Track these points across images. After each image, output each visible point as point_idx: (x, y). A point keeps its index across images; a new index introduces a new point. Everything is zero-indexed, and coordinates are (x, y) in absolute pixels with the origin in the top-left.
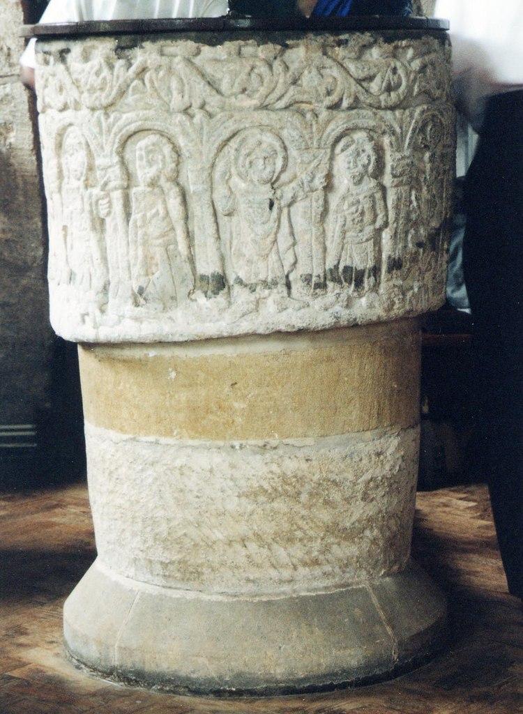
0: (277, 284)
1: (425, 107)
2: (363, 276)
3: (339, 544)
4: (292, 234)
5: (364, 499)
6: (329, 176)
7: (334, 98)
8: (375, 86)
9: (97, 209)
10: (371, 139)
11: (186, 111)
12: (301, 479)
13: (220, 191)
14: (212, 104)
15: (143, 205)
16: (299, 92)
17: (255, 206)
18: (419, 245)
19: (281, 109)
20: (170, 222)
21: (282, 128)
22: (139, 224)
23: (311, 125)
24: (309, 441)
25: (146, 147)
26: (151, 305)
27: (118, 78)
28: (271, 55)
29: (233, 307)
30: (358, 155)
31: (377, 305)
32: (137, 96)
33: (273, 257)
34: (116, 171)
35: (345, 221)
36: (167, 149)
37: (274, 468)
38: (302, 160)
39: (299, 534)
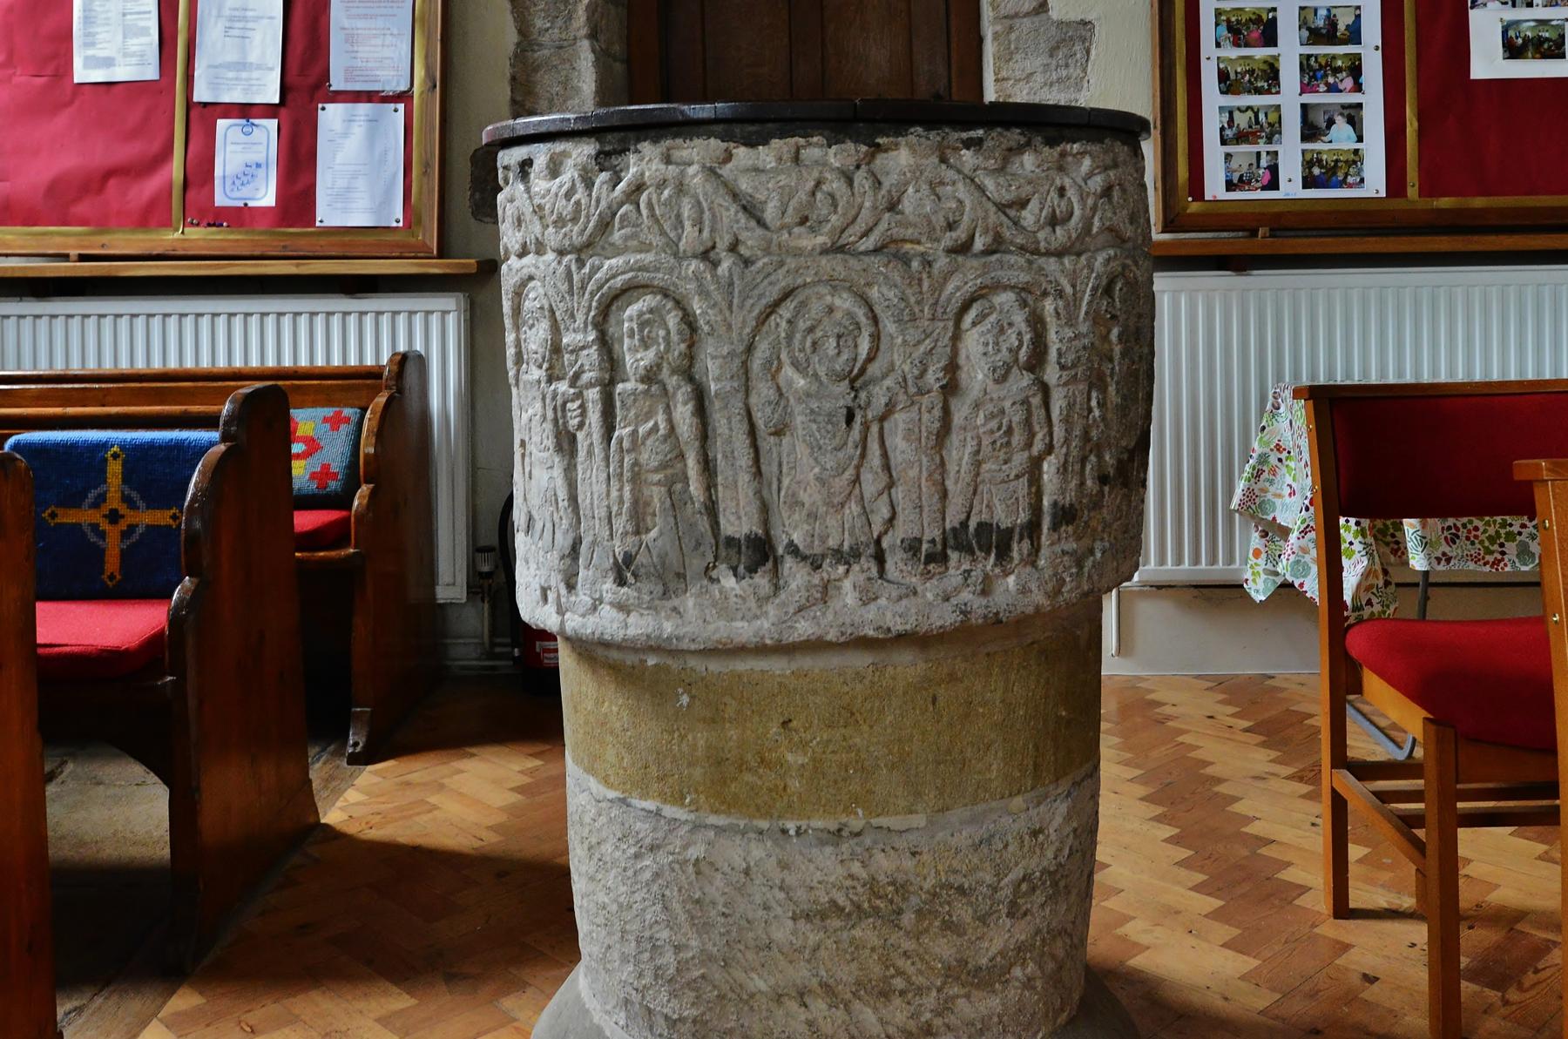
0: (859, 556)
1: (1112, 252)
2: (1011, 538)
3: (968, 996)
4: (887, 467)
5: (1010, 915)
6: (952, 367)
7: (960, 234)
8: (1028, 217)
9: (564, 417)
10: (1024, 304)
11: (707, 255)
12: (902, 888)
13: (763, 391)
14: (749, 243)
16: (899, 224)
17: (820, 419)
18: (1103, 479)
19: (866, 253)
20: (677, 444)
21: (869, 284)
22: (626, 445)
23: (920, 280)
24: (919, 820)
26: (646, 586)
27: (598, 201)
28: (850, 163)
29: (783, 596)
30: (1002, 331)
31: (1033, 586)
32: (627, 231)
33: (854, 508)
34: (591, 356)
35: (979, 444)
36: (673, 320)
37: (856, 868)
38: (905, 341)
39: (899, 983)
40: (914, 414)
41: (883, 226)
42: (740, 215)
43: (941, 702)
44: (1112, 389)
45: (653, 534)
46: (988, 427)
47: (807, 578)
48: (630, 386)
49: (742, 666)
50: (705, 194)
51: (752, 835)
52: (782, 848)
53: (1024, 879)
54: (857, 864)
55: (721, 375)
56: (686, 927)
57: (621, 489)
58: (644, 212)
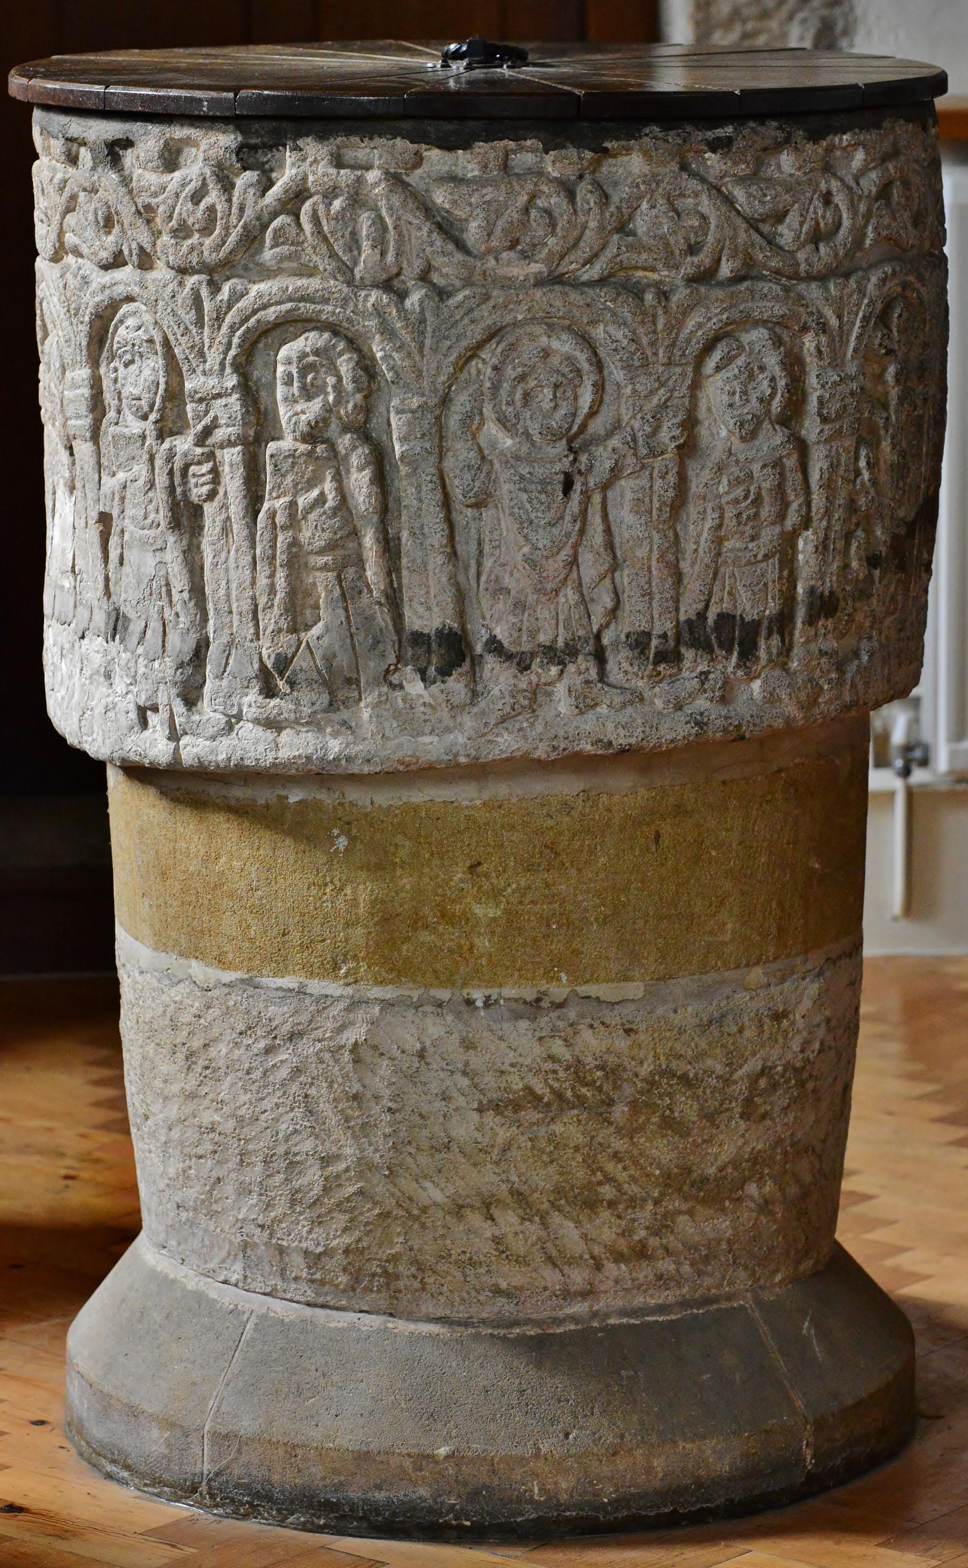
1: (888, 269)
2: (757, 634)
3: (690, 1213)
4: (610, 545)
5: (744, 1116)
6: (690, 423)
7: (704, 258)
8: (786, 233)
9: (185, 482)
10: (778, 342)
12: (613, 1073)
13: (460, 453)
15: (289, 479)
16: (630, 247)
18: (873, 561)
19: (590, 284)
21: (593, 323)
22: (280, 519)
23: (654, 316)
24: (635, 989)
27: (242, 209)
33: (569, 594)
35: (721, 517)
36: (345, 365)
37: (558, 1047)
38: (634, 391)
39: (607, 1191)
40: (644, 481)
41: (611, 251)
42: (435, 235)
43: (666, 841)
44: (886, 446)
45: (316, 630)
46: (732, 496)
47: (512, 681)
48: (287, 443)
49: (419, 795)
50: (390, 208)
51: (429, 1009)
52: (466, 1024)
53: (762, 1073)
54: (559, 1042)
56: (338, 1133)
57: (272, 576)
58: (307, 227)
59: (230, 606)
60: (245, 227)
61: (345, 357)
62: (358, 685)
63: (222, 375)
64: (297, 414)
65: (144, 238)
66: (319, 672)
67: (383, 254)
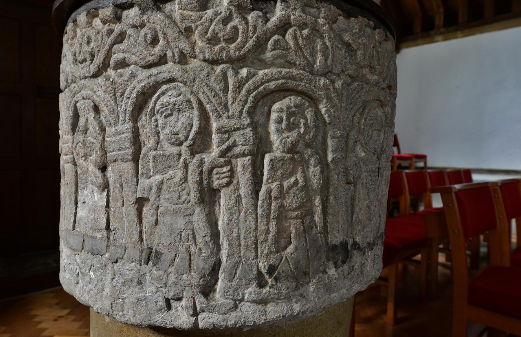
15: (279, 172)
25: (289, 107)
27: (255, 28)
36: (309, 114)
45: (291, 248)
55: (337, 149)
57: (268, 224)
58: (291, 42)
59: (240, 242)
60: (257, 38)
61: (310, 109)
62: (309, 275)
63: (240, 118)
64: (284, 138)
65: (185, 46)
66: (292, 271)
67: (326, 60)
